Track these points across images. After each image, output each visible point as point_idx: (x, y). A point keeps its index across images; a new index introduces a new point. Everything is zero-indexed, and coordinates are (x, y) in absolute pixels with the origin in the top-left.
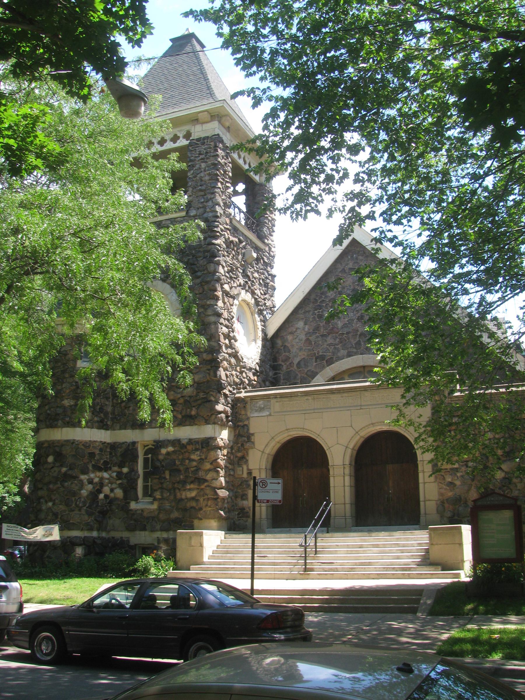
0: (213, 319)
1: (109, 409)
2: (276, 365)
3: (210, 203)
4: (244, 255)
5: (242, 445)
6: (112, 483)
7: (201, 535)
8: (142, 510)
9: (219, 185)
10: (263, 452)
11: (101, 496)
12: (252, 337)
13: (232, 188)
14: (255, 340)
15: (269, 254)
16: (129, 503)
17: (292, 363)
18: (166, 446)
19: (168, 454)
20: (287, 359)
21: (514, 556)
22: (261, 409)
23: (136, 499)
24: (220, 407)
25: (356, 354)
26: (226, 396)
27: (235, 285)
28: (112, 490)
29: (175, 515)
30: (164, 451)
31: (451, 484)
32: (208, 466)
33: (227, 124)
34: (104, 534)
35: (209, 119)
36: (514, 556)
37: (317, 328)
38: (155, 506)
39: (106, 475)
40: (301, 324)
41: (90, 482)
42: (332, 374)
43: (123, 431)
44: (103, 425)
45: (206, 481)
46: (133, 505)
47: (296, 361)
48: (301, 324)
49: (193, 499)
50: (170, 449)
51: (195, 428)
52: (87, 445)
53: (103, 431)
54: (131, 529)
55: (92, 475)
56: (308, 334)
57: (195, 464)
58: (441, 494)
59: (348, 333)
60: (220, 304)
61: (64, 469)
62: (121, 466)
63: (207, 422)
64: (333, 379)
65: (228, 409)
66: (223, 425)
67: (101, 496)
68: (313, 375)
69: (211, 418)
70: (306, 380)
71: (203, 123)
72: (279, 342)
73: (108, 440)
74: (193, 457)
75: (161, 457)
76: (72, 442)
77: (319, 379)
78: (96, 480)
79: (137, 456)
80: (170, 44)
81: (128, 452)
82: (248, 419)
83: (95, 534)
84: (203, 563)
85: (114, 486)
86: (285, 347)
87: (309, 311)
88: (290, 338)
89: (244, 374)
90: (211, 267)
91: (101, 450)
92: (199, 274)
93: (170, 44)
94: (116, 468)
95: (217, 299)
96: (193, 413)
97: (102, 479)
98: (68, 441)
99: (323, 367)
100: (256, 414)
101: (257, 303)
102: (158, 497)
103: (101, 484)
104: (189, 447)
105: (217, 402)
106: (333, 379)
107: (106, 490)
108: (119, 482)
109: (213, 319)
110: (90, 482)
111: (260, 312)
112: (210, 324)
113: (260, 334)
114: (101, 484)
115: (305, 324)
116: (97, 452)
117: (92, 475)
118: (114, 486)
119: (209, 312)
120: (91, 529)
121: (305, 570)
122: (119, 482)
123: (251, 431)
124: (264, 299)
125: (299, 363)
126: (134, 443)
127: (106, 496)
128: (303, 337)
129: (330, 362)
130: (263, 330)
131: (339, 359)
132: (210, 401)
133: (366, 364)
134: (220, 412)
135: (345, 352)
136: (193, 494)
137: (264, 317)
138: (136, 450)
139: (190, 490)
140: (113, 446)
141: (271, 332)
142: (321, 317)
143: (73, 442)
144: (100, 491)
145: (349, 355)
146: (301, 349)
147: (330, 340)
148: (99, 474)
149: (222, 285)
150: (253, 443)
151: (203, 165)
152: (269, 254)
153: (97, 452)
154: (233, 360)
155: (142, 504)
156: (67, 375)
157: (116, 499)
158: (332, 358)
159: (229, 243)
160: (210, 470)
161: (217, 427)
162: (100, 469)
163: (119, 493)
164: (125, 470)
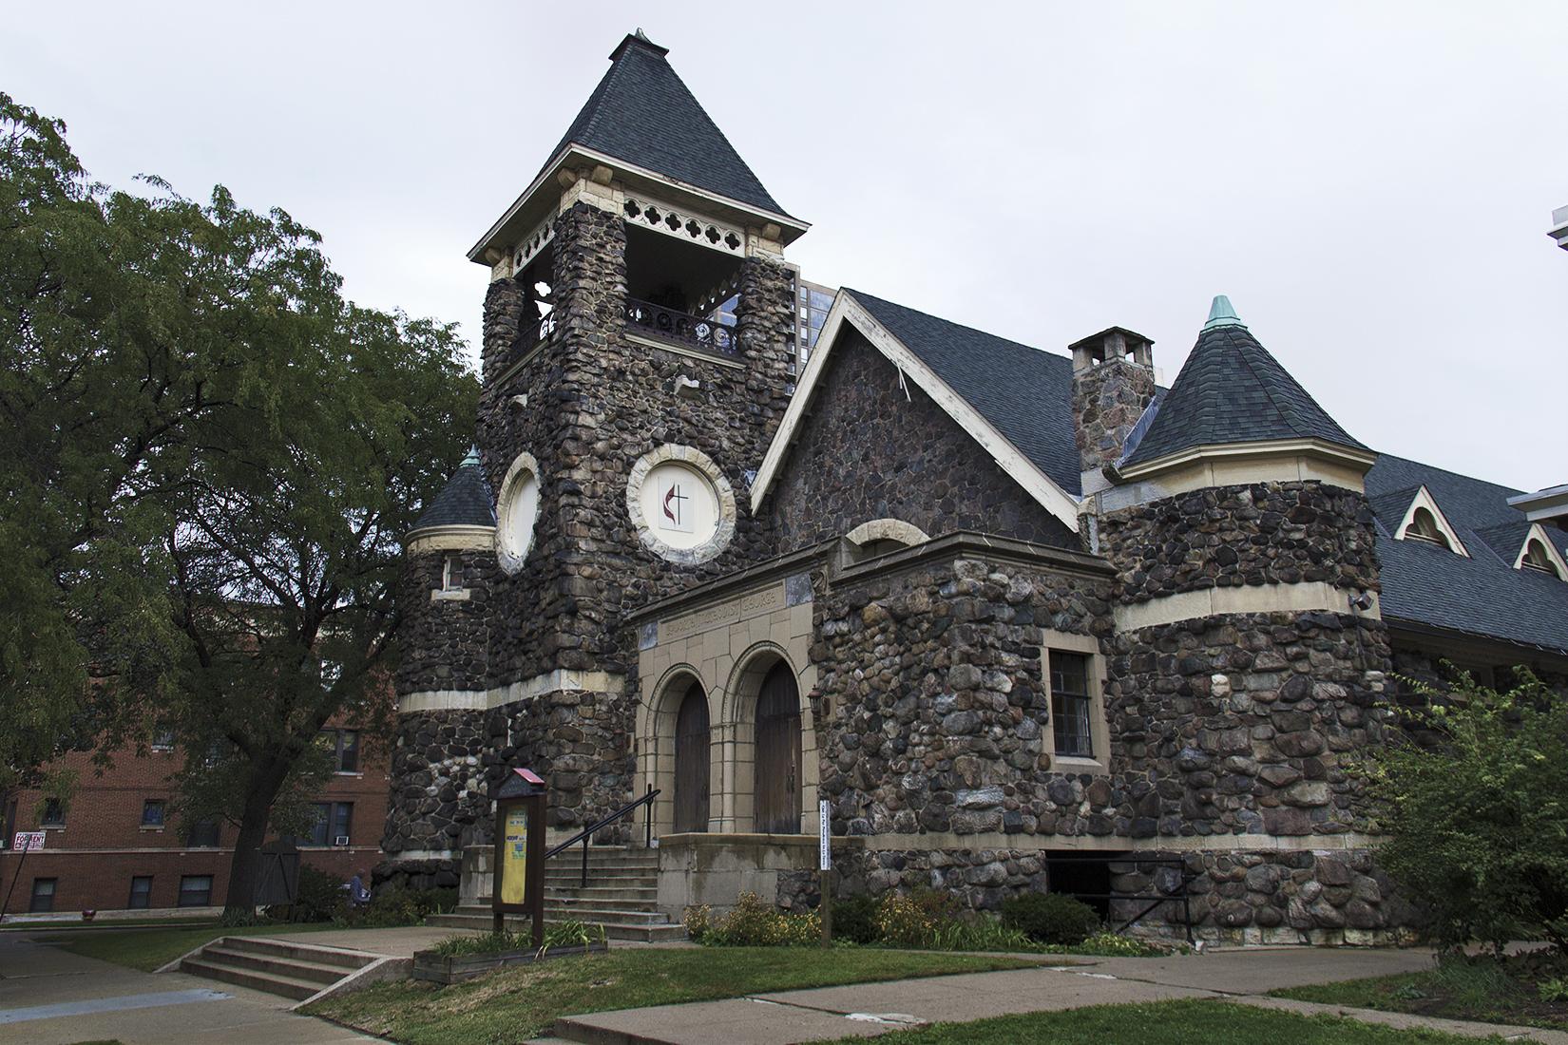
11: (463, 794)
25: (861, 522)
39: (471, 760)
52: (443, 716)
53: (470, 694)
55: (447, 762)
88: (788, 509)
97: (466, 766)
107: (472, 782)
110: (445, 772)
120: (438, 849)
142: (821, 466)
162: (464, 754)
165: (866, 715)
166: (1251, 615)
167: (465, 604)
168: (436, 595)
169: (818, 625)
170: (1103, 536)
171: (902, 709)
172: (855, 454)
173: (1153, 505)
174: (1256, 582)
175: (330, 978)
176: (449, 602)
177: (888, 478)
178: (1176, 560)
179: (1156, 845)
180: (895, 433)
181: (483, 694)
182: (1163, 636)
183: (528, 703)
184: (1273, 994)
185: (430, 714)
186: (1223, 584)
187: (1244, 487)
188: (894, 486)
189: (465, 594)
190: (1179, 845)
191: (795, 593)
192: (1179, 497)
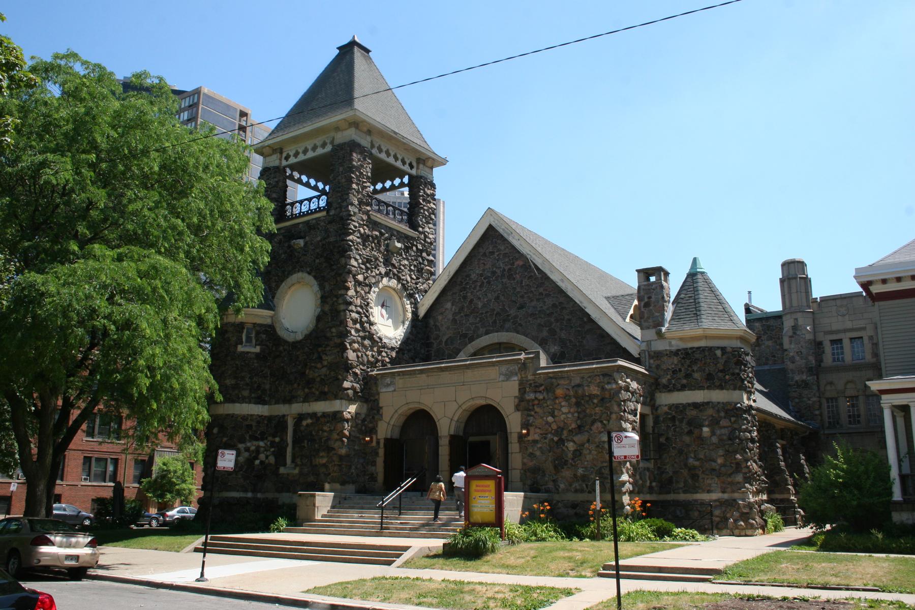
0: (342, 307)
1: (267, 387)
2: (422, 342)
3: (345, 204)
4: (387, 245)
5: (373, 417)
6: (266, 451)
7: (314, 496)
8: (288, 474)
9: (354, 186)
10: (389, 424)
11: (257, 462)
12: (401, 319)
13: (372, 187)
14: (403, 323)
15: (425, 241)
16: (278, 468)
17: (441, 341)
18: (306, 419)
19: (307, 425)
20: (438, 337)
21: (472, 520)
22: (388, 385)
23: (285, 465)
24: (346, 384)
25: (492, 332)
26: (355, 374)
27: (374, 274)
28: (267, 457)
29: (311, 478)
30: (304, 423)
31: (532, 455)
32: (335, 436)
33: (365, 129)
34: (259, 495)
35: (271, 152)
36: (472, 520)
37: (462, 309)
38: (296, 471)
39: (262, 444)
40: (449, 305)
41: (247, 449)
42: (472, 351)
43: (277, 406)
44: (260, 401)
45: (333, 449)
46: (282, 470)
47: (444, 340)
48: (449, 305)
49: (324, 465)
50: (309, 421)
51: (327, 402)
52: (245, 418)
53: (260, 406)
54: (280, 491)
55: (249, 444)
56: (455, 314)
57: (325, 434)
58: (524, 464)
59: (487, 312)
60: (351, 292)
61: (225, 439)
62: (274, 437)
63: (336, 397)
64: (475, 354)
65: (357, 386)
66: (351, 401)
67: (257, 462)
68: (457, 352)
69: (338, 393)
70: (453, 355)
71: (343, 130)
72: (431, 322)
73: (266, 413)
74: (325, 428)
75: (302, 428)
76: (232, 416)
77: (462, 356)
78: (253, 448)
79: (286, 427)
80: (338, 51)
81: (279, 424)
82: (378, 394)
83: (250, 495)
84: (315, 521)
85: (268, 453)
86: (436, 326)
87: (455, 293)
88: (440, 318)
89: (384, 354)
90: (343, 261)
91: (258, 422)
92: (334, 267)
93: (338, 51)
94: (270, 438)
95: (348, 289)
96: (326, 390)
97: (258, 447)
98: (228, 415)
99: (466, 345)
100: (384, 390)
101: (404, 287)
102: (299, 463)
103: (257, 451)
104: (322, 420)
105: (345, 379)
106: (475, 354)
107: (262, 456)
108: (272, 449)
109: (342, 307)
110: (247, 449)
111: (410, 296)
112: (340, 312)
113: (409, 315)
114: (257, 451)
115: (453, 305)
116: (254, 424)
117: (249, 444)
118: (268, 453)
119: (340, 301)
120: (246, 491)
121: (382, 528)
122: (272, 449)
123: (381, 405)
124: (416, 284)
125: (446, 342)
126: (284, 416)
127: (262, 462)
128: (450, 317)
129: (472, 340)
130: (413, 312)
131: (479, 336)
132: (338, 379)
133: (501, 341)
134: (348, 389)
135: (482, 330)
136: (324, 461)
137: (416, 299)
138: (286, 422)
139: (322, 457)
140: (270, 418)
141: (422, 312)
142: (465, 298)
143: (232, 416)
144: (256, 458)
145: (487, 333)
146: (448, 328)
147: (471, 320)
148: (256, 443)
149: (354, 276)
150: (382, 415)
151: (341, 169)
152: (425, 241)
153: (254, 424)
154: (367, 342)
155: (289, 469)
156: (229, 358)
157: (270, 464)
158: (473, 336)
159: (365, 238)
160: (337, 440)
161: (344, 402)
162: (257, 439)
163: (272, 460)
164: (277, 440)
165: (556, 439)
166: (719, 403)
167: (257, 355)
168: (240, 348)
169: (522, 391)
170: (652, 361)
171: (578, 438)
172: (489, 295)
173: (678, 350)
174: (721, 387)
175: (398, 556)
176: (248, 353)
177: (513, 312)
178: (688, 376)
179: (671, 497)
180: (518, 289)
181: (266, 407)
182: (680, 409)
183: (313, 415)
184: (308, 591)
185: (238, 416)
186: (709, 388)
187: (718, 348)
188: (516, 317)
189: (258, 349)
190: (682, 497)
191: (506, 375)
192: (691, 348)
